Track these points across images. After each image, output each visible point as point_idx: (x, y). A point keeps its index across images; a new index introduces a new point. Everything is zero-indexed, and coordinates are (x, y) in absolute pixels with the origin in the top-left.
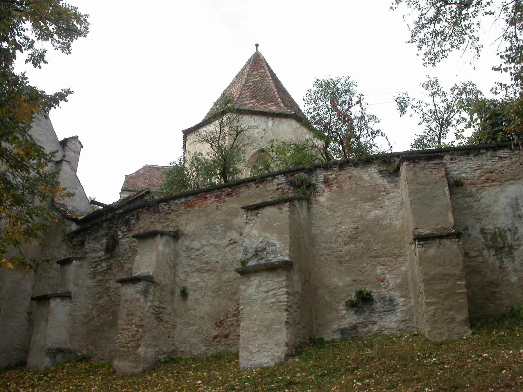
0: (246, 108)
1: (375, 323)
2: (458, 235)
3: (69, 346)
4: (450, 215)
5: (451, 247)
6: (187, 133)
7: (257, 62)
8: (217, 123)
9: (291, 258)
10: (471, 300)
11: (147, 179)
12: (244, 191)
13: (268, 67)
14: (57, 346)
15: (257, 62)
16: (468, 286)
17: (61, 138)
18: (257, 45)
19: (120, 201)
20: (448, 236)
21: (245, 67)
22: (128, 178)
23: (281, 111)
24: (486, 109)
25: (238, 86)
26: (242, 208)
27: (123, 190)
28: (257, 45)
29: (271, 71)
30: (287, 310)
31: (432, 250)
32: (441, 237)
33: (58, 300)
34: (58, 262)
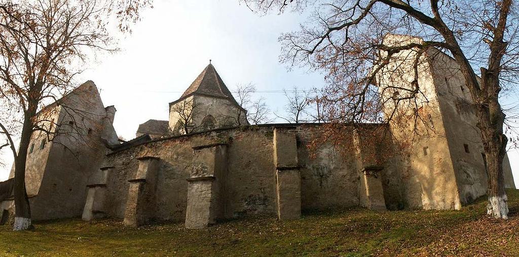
0: (203, 93)
1: (256, 210)
2: (298, 168)
3: (104, 211)
4: (296, 158)
5: (295, 174)
6: (171, 104)
7: (210, 70)
8: (183, 102)
9: (214, 175)
10: (302, 201)
11: (150, 126)
12: (195, 139)
13: (216, 72)
14: (98, 210)
15: (210, 70)
16: (302, 194)
17: (105, 107)
18: (210, 60)
19: (137, 138)
20: (293, 169)
21: (204, 71)
22: (151, 123)
23: (220, 95)
24: (178, 155)
25: (200, 81)
26: (193, 148)
27: (138, 132)
28: (210, 60)
29: (217, 74)
30: (210, 201)
31: (286, 174)
32: (290, 169)
33: (99, 188)
34: (101, 169)
